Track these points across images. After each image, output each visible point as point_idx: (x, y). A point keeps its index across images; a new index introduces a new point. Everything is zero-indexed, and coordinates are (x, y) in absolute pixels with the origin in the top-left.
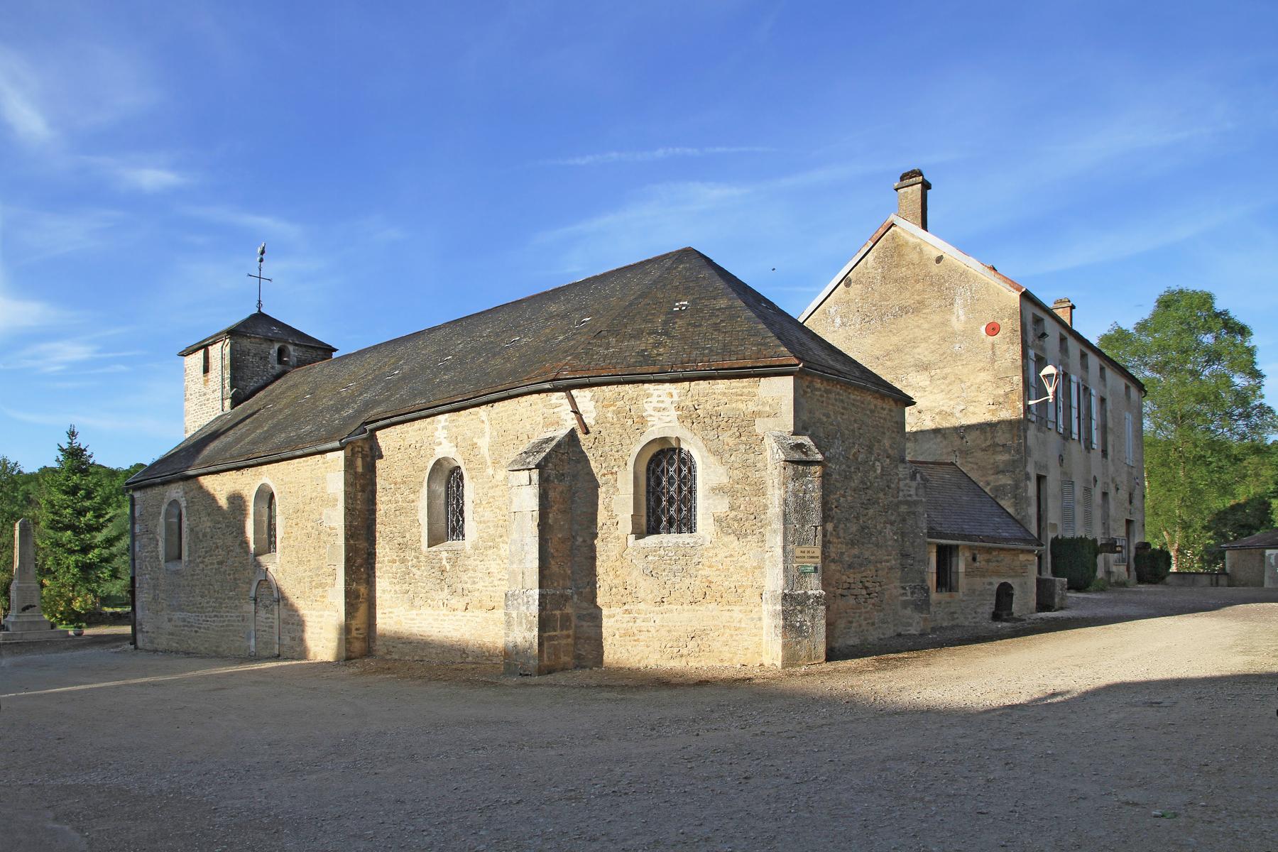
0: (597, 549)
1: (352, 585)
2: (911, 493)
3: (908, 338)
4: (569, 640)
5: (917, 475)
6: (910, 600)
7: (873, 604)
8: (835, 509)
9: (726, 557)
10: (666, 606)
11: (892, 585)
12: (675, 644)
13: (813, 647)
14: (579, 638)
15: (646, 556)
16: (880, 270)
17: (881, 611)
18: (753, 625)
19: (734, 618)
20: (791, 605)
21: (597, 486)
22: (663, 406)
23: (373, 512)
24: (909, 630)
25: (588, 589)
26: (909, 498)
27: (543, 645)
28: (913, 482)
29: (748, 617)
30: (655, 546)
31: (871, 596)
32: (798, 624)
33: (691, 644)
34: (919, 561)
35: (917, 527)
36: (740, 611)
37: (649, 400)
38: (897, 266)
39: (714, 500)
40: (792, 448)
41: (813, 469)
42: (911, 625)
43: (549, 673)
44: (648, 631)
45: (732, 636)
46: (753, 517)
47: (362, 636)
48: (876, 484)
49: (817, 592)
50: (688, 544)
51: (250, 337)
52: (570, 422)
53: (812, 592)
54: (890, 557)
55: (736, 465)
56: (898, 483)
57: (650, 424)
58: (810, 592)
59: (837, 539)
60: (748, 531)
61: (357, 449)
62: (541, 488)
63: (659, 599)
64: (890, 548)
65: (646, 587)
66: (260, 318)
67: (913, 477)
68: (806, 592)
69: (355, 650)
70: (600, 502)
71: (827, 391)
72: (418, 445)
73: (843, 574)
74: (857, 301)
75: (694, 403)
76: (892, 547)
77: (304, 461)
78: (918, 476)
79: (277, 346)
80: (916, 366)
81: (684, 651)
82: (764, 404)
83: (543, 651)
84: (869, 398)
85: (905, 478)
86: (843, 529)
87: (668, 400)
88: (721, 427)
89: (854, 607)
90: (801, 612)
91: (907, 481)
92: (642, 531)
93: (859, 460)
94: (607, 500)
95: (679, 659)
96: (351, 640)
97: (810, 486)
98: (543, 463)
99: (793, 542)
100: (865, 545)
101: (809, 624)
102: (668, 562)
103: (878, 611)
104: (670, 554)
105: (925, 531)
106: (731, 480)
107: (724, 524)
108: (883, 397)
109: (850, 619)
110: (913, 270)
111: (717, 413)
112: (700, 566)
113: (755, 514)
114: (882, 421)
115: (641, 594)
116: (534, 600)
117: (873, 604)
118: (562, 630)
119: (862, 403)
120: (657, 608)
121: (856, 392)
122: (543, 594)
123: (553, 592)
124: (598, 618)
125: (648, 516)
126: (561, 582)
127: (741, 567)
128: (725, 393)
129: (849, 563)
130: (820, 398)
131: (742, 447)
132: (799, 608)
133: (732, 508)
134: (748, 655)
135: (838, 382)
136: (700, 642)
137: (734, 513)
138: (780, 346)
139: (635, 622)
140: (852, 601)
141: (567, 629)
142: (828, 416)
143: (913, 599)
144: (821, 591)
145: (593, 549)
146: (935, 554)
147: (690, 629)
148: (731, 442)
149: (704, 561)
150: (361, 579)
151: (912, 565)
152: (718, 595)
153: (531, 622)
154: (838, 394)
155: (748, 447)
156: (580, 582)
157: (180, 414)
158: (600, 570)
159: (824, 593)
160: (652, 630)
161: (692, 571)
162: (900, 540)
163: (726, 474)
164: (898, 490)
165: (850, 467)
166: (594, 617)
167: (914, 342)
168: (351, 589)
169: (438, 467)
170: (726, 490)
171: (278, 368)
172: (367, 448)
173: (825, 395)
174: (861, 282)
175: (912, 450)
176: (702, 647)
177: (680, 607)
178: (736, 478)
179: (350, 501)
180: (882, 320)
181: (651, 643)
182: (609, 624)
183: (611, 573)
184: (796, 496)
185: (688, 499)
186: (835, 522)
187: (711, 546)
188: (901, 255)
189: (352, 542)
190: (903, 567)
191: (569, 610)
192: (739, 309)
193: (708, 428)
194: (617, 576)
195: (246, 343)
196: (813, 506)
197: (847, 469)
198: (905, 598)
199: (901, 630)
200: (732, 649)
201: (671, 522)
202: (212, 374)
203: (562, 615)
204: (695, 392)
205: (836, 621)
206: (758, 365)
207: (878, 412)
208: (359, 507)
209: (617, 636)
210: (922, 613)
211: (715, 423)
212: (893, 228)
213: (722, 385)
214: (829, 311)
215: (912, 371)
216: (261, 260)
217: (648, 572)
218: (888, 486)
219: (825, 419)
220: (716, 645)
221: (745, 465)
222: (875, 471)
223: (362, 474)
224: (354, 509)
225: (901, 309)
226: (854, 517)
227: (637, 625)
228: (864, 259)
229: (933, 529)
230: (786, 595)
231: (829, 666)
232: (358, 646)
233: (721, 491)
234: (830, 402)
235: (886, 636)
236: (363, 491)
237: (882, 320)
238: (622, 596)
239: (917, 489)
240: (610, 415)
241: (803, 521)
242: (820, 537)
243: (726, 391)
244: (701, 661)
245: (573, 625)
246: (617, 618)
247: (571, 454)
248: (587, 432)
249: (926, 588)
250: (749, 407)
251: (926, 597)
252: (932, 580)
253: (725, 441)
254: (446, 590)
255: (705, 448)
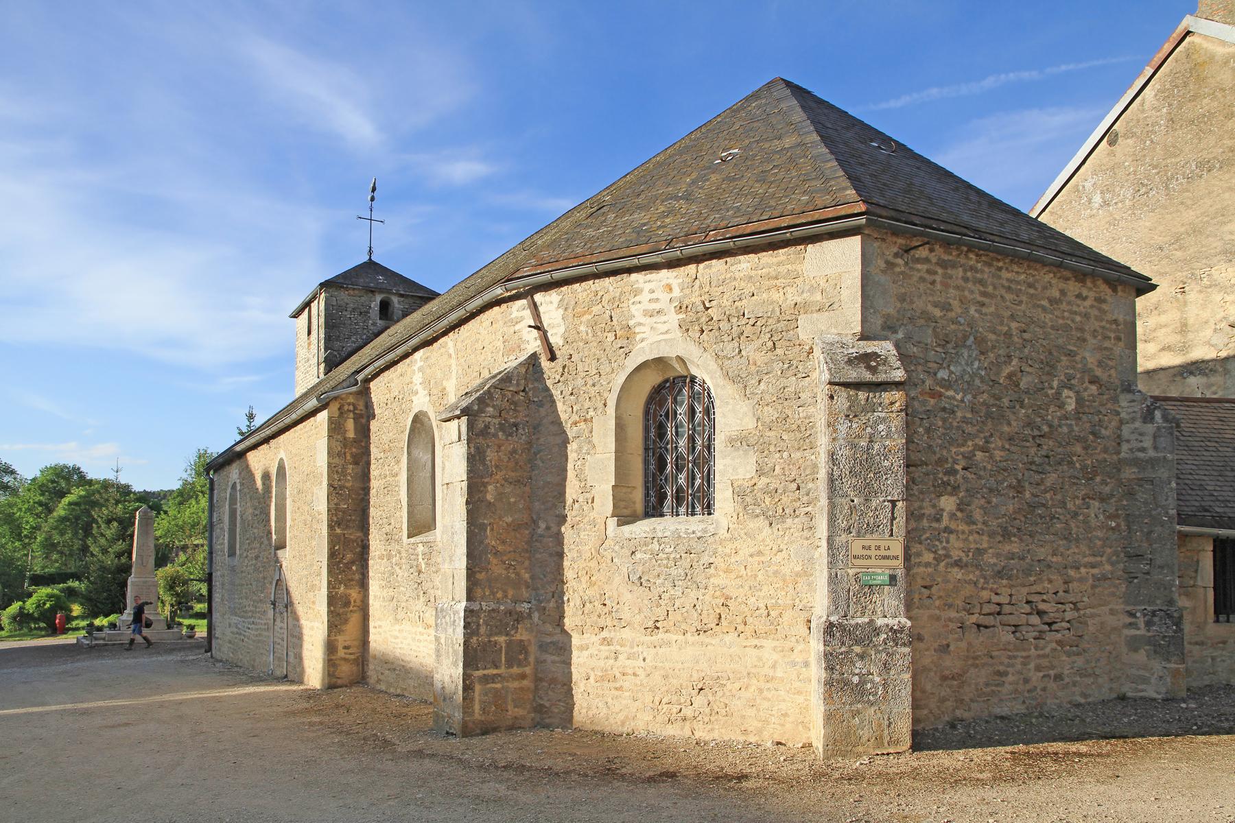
0: (566, 541)
1: (339, 588)
2: (1145, 445)
3: (1212, 210)
4: (525, 683)
5: (1156, 412)
6: (1144, 635)
7: (1059, 643)
8: (962, 473)
9: (751, 556)
10: (661, 635)
11: (1106, 609)
12: (674, 698)
13: (886, 722)
14: (541, 680)
15: (633, 553)
16: (1165, 110)
17: (1078, 654)
18: (795, 672)
19: (764, 660)
20: (843, 644)
21: (566, 441)
22: (657, 306)
23: (366, 490)
24: (1145, 691)
25: (552, 604)
26: (1141, 455)
27: (473, 689)
28: (1150, 425)
29: (786, 660)
30: (645, 535)
31: (1054, 627)
32: (856, 679)
33: (699, 701)
34: (1161, 567)
35: (1157, 506)
36: (774, 649)
37: (637, 299)
38: (1195, 98)
39: (733, 459)
40: (850, 362)
41: (887, 397)
42: (1145, 681)
43: (485, 732)
44: (635, 674)
45: (761, 691)
46: (794, 486)
47: (352, 657)
48: (1065, 429)
49: (896, 621)
50: (694, 532)
51: (347, 289)
52: (533, 343)
53: (886, 621)
54: (1099, 559)
55: (768, 398)
56: (1119, 428)
57: (638, 337)
58: (880, 622)
59: (968, 524)
60: (787, 511)
61: (346, 408)
62: (472, 445)
63: (650, 624)
64: (1099, 543)
65: (630, 601)
66: (371, 266)
67: (1148, 417)
68: (872, 621)
69: (342, 675)
70: (570, 466)
71: (943, 264)
72: (400, 397)
73: (983, 588)
74: (1127, 164)
75: (703, 298)
76: (1105, 540)
77: (301, 429)
78: (1158, 414)
79: (379, 298)
80: (1225, 252)
81: (688, 712)
82: (812, 290)
83: (472, 700)
84: (1048, 277)
85: (1133, 420)
86: (982, 507)
87: (665, 297)
88: (745, 334)
89: (1011, 647)
90: (861, 657)
91: (1138, 424)
92: (635, 511)
93: (1023, 385)
94: (579, 463)
95: (680, 723)
96: (337, 662)
97: (881, 427)
98: (476, 407)
99: (848, 530)
100: (1038, 537)
101: (877, 679)
102: (665, 562)
103: (1069, 655)
104: (667, 550)
105: (1173, 512)
106: (759, 424)
107: (748, 499)
108: (1081, 277)
109: (1001, 668)
110: (1222, 100)
111: (738, 311)
112: (712, 571)
113: (798, 481)
114: (1078, 319)
115: (626, 615)
116: (459, 618)
117: (1059, 643)
118: (510, 664)
119: (1030, 286)
120: (649, 638)
121: (1016, 268)
122: (472, 611)
123: (493, 606)
124: (565, 650)
125: (647, 489)
126: (511, 593)
127: (776, 573)
128: (751, 277)
129: (998, 568)
130: (927, 277)
131: (777, 367)
132: (857, 649)
133: (760, 472)
134: (788, 726)
135: (971, 247)
136: (711, 698)
137: (764, 480)
138: (845, 189)
139: (616, 659)
140: (1007, 636)
141: (520, 665)
142: (946, 307)
143: (1150, 634)
144: (904, 620)
145: (559, 539)
146: (1210, 555)
147: (695, 676)
148: (761, 358)
149: (718, 561)
150: (352, 580)
151: (1148, 573)
152: (739, 620)
153: (455, 651)
154: (972, 268)
155: (786, 366)
156: (543, 592)
157: (292, 384)
158: (569, 574)
159: (909, 623)
160: (640, 672)
161: (700, 578)
162: (1123, 527)
163: (751, 414)
164: (1119, 440)
165: (999, 399)
166: (561, 648)
167: (1223, 215)
168: (337, 593)
169: (418, 425)
170: (752, 441)
171: (380, 323)
172: (361, 406)
173: (940, 271)
174: (1134, 135)
175: (1219, 387)
176: (715, 708)
177: (681, 637)
178: (768, 420)
179: (336, 476)
180: (1167, 187)
181: (640, 695)
182: (581, 660)
183: (584, 579)
184: (854, 446)
185: (703, 460)
186: (961, 495)
187: (729, 536)
188: (1201, 80)
189: (338, 531)
190: (1130, 577)
191: (522, 635)
192: (809, 145)
193: (726, 338)
194: (592, 584)
195: (343, 296)
196: (886, 463)
197: (992, 401)
198: (1133, 632)
199: (1128, 689)
200: (761, 713)
201: (679, 499)
202: (314, 333)
203: (509, 644)
204: (706, 280)
205: (965, 672)
206: (799, 221)
207: (1069, 303)
208: (349, 485)
209: (592, 680)
210: (1169, 661)
211: (735, 328)
212: (1188, 39)
213: (745, 264)
214: (1084, 187)
215: (1219, 261)
216: (373, 199)
217: (634, 578)
218: (1093, 433)
219: (937, 313)
220: (736, 704)
221: (782, 397)
222: (1061, 406)
223: (355, 441)
224: (342, 487)
225: (1200, 165)
226: (1010, 486)
227: (619, 663)
228: (1139, 98)
229: (1206, 511)
230: (831, 625)
231: (912, 761)
232: (345, 670)
233: (744, 443)
234: (952, 283)
235: (1090, 700)
236: (356, 463)
237: (1167, 187)
238: (599, 616)
239: (1155, 437)
240: (582, 328)
241: (868, 492)
242: (901, 520)
243: (753, 273)
244: (712, 730)
245: (532, 659)
246: (592, 650)
247: (530, 394)
248: (553, 358)
249: (1176, 615)
250: (789, 296)
251: (1175, 632)
252: (1206, 602)
253: (750, 359)
254: (422, 599)
255: (719, 373)
